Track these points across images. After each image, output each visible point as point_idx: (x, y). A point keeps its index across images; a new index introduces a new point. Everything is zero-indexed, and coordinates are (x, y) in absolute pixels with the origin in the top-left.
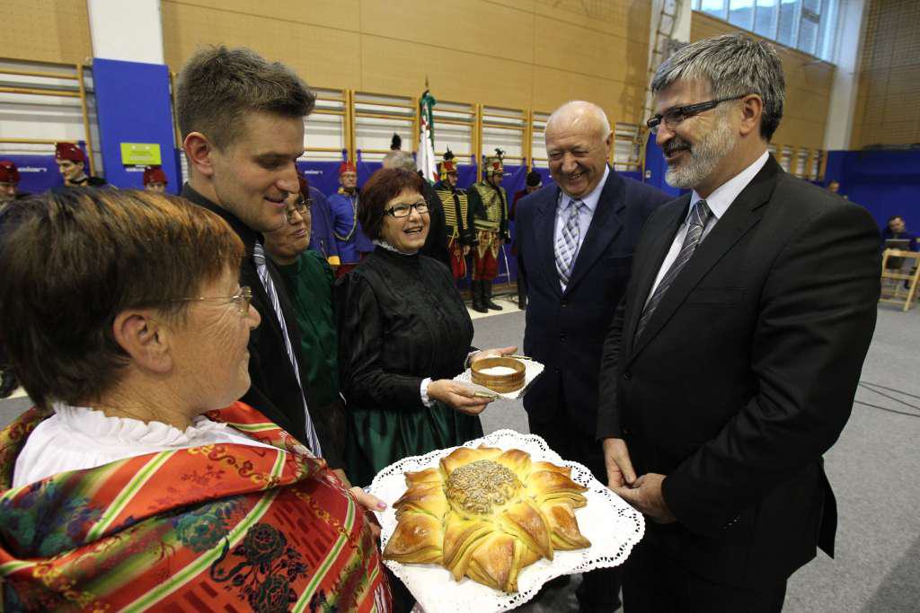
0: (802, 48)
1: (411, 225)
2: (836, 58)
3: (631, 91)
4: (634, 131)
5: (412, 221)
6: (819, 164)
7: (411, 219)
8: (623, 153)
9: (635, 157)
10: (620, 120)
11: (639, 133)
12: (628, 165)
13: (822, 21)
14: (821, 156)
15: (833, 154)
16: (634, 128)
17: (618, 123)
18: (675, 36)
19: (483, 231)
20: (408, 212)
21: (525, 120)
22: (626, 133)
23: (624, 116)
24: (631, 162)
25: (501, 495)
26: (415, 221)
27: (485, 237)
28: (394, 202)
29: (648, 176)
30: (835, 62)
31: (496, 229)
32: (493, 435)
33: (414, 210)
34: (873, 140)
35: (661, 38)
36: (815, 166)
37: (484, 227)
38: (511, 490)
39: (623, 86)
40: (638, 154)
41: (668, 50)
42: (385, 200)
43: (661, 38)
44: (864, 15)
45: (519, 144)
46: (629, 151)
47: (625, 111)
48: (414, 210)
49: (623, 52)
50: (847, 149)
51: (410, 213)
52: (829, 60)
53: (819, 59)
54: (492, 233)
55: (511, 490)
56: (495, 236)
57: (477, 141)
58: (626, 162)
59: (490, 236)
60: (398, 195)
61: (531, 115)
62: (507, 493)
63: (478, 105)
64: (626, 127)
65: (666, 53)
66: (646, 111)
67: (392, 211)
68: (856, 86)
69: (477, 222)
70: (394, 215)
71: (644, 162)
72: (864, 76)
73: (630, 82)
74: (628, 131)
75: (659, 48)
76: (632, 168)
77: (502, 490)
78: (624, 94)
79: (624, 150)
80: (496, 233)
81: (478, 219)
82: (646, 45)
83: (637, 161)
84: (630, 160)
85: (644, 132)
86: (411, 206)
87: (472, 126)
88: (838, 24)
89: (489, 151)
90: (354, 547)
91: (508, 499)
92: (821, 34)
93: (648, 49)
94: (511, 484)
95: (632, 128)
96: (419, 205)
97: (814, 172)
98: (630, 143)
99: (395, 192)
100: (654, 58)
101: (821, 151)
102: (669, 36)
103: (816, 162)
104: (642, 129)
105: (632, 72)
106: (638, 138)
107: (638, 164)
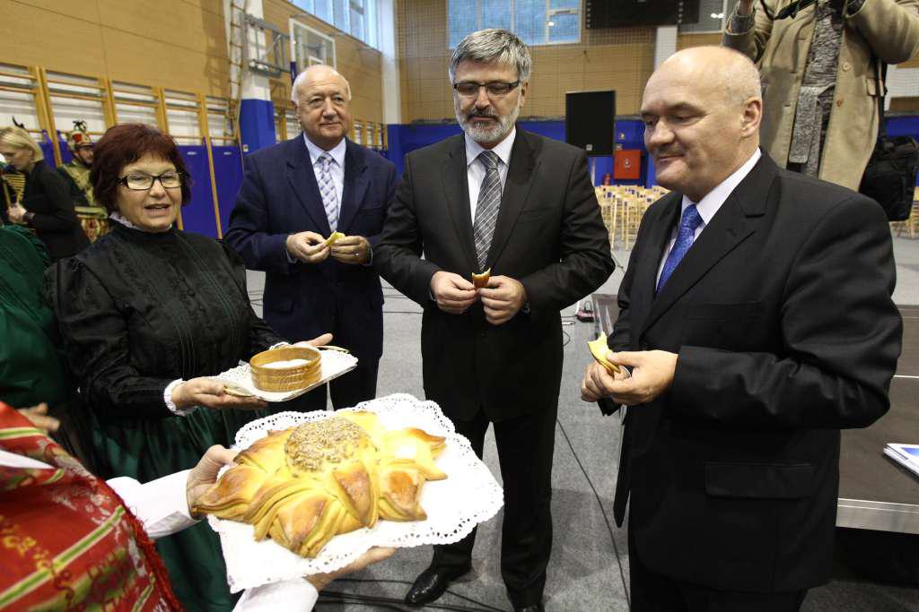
0: (354, 35)
1: (152, 202)
2: (380, 44)
3: (214, 63)
4: (225, 105)
5: (154, 197)
6: (382, 136)
7: (152, 193)
8: (216, 127)
9: (229, 132)
10: (209, 94)
11: (230, 108)
12: (225, 140)
13: (365, 13)
14: (382, 129)
15: (391, 127)
16: (224, 102)
17: (207, 97)
18: (249, 11)
19: (87, 219)
20: (150, 184)
21: (103, 90)
22: (216, 107)
23: (211, 91)
24: (227, 137)
25: (337, 452)
26: (157, 197)
27: (91, 226)
28: (129, 169)
29: (246, 150)
30: (380, 50)
31: (103, 215)
32: (390, 397)
33: (157, 182)
34: (418, 115)
35: (236, 11)
36: (380, 138)
37: (87, 214)
38: (350, 449)
39: (204, 58)
40: (232, 128)
41: (246, 24)
42: (118, 166)
43: (236, 11)
44: (394, 13)
45: (100, 118)
46: (222, 124)
47: (212, 84)
48: (157, 182)
49: (199, 21)
50: (400, 123)
51: (152, 185)
52: (376, 48)
53: (367, 46)
54: (99, 220)
55: (350, 449)
56: (103, 223)
57: (45, 113)
58: (222, 136)
59: (98, 223)
60: (136, 160)
61: (109, 83)
62: (345, 450)
63: (37, 69)
64: (217, 101)
65: (243, 26)
66: (233, 84)
67: (125, 182)
68: (398, 71)
69: (79, 209)
70: (127, 186)
71: (239, 137)
72: (402, 63)
73: (211, 53)
74: (219, 104)
75: (236, 21)
76: (229, 143)
77: (340, 447)
78: (208, 66)
79: (217, 124)
80: (104, 220)
81: (78, 206)
82: (222, 17)
83: (233, 136)
84: (225, 134)
85: (234, 107)
86: (155, 178)
87: (35, 94)
88: (376, 16)
89: (65, 125)
90: (64, 588)
91: (346, 457)
92: (366, 21)
93: (224, 23)
94: (353, 441)
95: (221, 102)
96: (168, 178)
97: (380, 143)
98: (223, 117)
99: (133, 157)
100: (232, 31)
101: (382, 125)
102: (244, 11)
103: (380, 134)
104: (232, 102)
105: (212, 43)
106: (230, 112)
107: (234, 138)
